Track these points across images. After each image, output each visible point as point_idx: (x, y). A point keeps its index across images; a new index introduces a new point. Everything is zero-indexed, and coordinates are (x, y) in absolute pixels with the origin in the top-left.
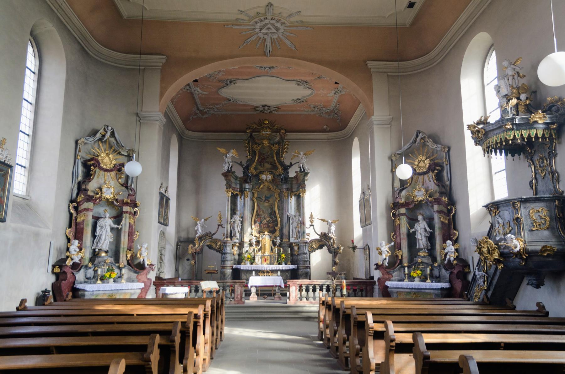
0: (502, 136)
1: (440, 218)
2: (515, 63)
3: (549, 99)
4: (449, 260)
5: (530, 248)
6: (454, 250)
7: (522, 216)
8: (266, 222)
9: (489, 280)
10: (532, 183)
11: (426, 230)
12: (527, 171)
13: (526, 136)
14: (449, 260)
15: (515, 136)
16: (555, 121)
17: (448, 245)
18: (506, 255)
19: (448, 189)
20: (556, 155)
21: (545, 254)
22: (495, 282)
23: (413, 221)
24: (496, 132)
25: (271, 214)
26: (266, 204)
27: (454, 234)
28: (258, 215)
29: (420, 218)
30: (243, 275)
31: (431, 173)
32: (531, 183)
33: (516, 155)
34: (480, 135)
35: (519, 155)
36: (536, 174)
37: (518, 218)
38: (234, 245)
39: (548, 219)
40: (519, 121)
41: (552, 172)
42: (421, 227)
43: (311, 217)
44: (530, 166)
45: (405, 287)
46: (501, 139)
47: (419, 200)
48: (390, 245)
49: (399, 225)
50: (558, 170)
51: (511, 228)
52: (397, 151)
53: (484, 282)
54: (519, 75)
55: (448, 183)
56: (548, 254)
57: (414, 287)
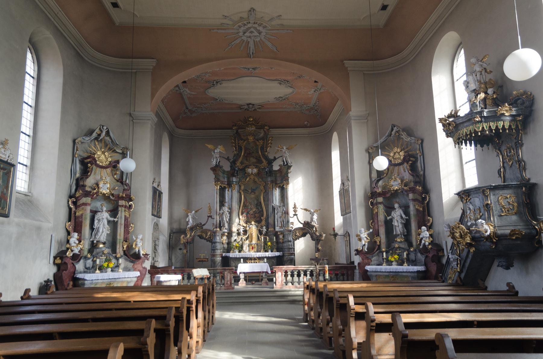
0: (471, 128)
2: (483, 59)
3: (515, 93)
4: (424, 244)
5: (499, 232)
6: (428, 235)
7: (491, 203)
8: (252, 213)
9: (462, 262)
10: (501, 172)
11: (402, 217)
12: (497, 161)
13: (493, 128)
14: (424, 244)
15: (483, 128)
16: (520, 113)
17: (423, 230)
18: (477, 239)
19: (422, 179)
20: (522, 145)
21: (514, 238)
22: (467, 265)
23: (389, 209)
24: (465, 124)
25: (257, 205)
26: (253, 196)
27: (429, 220)
28: (245, 206)
29: (396, 206)
30: (232, 262)
31: (405, 164)
32: (499, 171)
33: (485, 146)
34: (450, 127)
35: (488, 145)
36: (503, 163)
37: (488, 204)
38: (223, 235)
39: (516, 204)
40: (487, 114)
41: (519, 161)
43: (295, 207)
44: (498, 156)
46: (470, 131)
48: (369, 232)
49: (377, 213)
50: (525, 159)
51: (481, 214)
53: (457, 265)
54: (486, 71)
55: (422, 173)
56: (516, 238)
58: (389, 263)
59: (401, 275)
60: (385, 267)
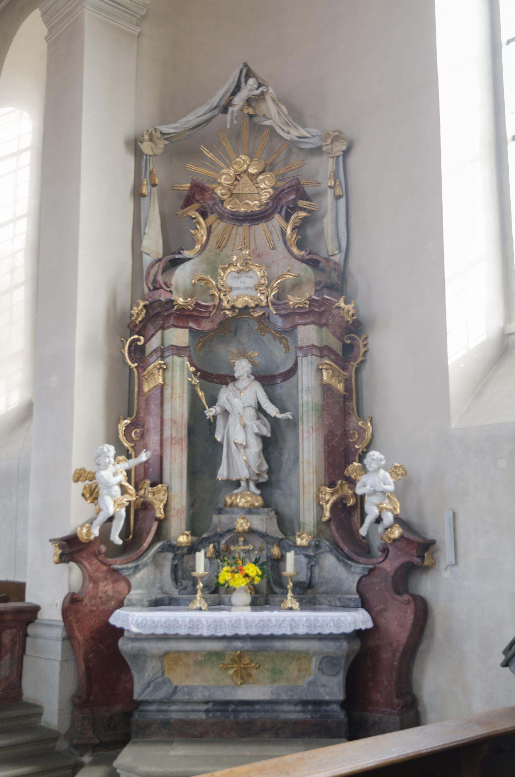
1: (320, 371)
11: (260, 410)
23: (213, 377)
29: (242, 368)
31: (277, 220)
42: (241, 407)
45: (205, 633)
47: (240, 304)
48: (133, 462)
49: (162, 388)
52: (164, 122)
57: (242, 632)
58: (218, 594)
59: (278, 651)
60: (196, 618)
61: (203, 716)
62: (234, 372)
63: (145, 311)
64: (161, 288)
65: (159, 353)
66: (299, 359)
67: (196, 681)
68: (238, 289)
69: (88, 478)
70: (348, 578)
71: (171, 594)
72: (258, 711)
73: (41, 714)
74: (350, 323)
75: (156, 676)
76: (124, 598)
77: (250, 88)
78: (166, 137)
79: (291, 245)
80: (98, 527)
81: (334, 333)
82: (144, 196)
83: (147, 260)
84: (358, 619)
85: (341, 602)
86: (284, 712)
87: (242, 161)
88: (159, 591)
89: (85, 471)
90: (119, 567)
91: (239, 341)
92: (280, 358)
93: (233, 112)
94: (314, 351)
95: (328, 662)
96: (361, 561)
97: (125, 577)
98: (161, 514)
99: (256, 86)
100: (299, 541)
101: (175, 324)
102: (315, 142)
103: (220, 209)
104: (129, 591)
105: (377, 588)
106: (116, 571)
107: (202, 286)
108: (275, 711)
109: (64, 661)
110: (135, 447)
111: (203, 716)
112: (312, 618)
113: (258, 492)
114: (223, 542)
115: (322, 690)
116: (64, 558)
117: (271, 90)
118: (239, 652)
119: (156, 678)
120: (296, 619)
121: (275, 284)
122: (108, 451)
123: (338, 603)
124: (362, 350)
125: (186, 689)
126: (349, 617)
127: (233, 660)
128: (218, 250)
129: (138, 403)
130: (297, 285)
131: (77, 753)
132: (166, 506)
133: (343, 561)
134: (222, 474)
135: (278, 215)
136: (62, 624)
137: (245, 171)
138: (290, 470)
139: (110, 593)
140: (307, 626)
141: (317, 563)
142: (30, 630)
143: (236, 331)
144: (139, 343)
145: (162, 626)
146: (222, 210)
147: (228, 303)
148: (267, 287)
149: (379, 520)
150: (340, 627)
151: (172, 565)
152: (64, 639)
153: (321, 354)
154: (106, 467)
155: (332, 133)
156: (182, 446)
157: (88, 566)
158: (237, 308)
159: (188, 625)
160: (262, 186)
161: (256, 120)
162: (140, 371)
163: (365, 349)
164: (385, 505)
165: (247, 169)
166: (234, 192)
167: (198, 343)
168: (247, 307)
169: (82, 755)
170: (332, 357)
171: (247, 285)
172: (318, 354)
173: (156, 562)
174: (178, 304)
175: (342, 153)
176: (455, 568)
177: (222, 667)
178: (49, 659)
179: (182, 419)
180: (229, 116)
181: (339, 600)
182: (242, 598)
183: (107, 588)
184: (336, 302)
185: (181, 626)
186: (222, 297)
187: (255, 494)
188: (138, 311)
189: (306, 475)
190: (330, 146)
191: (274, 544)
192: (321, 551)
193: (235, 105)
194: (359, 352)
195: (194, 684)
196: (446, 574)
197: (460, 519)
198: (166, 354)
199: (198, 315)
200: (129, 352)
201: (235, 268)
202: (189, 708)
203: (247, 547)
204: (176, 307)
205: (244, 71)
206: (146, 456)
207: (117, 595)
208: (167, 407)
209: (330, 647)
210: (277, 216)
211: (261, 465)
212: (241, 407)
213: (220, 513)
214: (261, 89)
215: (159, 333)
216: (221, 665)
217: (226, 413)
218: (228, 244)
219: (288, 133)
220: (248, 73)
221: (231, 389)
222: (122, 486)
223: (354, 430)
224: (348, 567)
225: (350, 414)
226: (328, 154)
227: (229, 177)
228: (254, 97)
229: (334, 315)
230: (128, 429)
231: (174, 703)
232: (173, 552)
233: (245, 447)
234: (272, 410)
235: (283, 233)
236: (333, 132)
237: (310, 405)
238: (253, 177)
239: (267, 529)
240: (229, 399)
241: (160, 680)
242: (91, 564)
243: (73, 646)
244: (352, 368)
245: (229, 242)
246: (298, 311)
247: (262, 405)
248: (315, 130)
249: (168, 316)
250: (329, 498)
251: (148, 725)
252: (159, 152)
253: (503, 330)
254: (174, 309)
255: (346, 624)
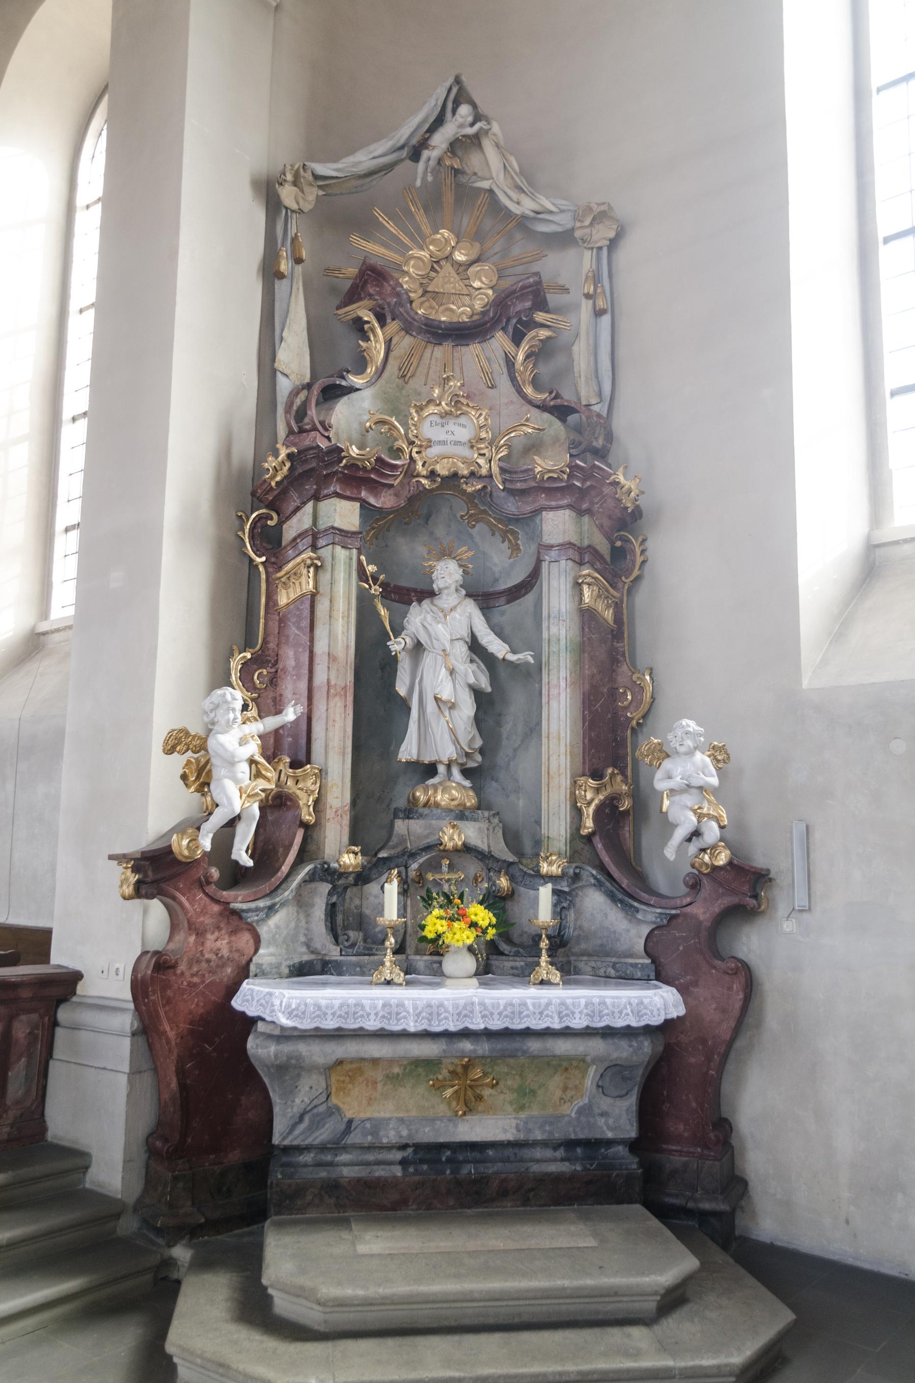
11: (475, 647)
29: (447, 574)
31: (500, 341)
47: (443, 470)
48: (272, 723)
57: (477, 1024)
58: (421, 956)
61: (398, 1171)
62: (432, 582)
63: (288, 465)
64: (315, 429)
65: (309, 540)
66: (545, 565)
67: (385, 1110)
68: (443, 443)
69: (191, 747)
70: (628, 931)
71: (325, 955)
72: (493, 1161)
73: (87, 1168)
74: (630, 510)
75: (315, 1102)
76: (251, 960)
77: (460, 120)
78: (321, 183)
79: (524, 382)
80: (211, 835)
81: (601, 527)
82: (281, 276)
83: (284, 386)
84: (660, 1002)
85: (617, 971)
86: (538, 1161)
87: (443, 240)
88: (304, 949)
89: (187, 734)
90: (244, 906)
91: (432, 533)
92: (504, 565)
93: (429, 159)
94: (571, 552)
95: (615, 1072)
96: (652, 902)
97: (250, 924)
98: (310, 815)
99: (470, 119)
100: (545, 868)
101: (338, 491)
102: (564, 221)
103: (408, 313)
104: (256, 950)
105: (681, 948)
106: (237, 914)
107: (381, 433)
108: (522, 1160)
109: (135, 1072)
110: (259, 700)
111: (398, 1171)
112: (596, 1001)
113: (467, 783)
114: (414, 866)
115: (601, 1121)
116: (141, 891)
117: (496, 128)
118: (466, 1060)
119: (315, 1107)
120: (569, 1001)
121: (502, 442)
122: (234, 699)
123: (612, 972)
124: (639, 559)
125: (368, 1125)
126: (657, 999)
127: (453, 1073)
128: (401, 381)
129: (266, 625)
130: (533, 447)
131: (160, 1241)
132: (317, 802)
133: (621, 901)
134: (408, 751)
135: (501, 333)
136: (131, 1006)
137: (447, 258)
138: (515, 750)
139: (225, 952)
140: (587, 1015)
141: (572, 904)
142: (64, 1014)
143: (428, 518)
144: (269, 522)
145: (334, 1014)
146: (409, 316)
147: (423, 465)
148: (491, 444)
149: (697, 833)
150: (642, 1016)
151: (327, 904)
152: (134, 1034)
153: (581, 559)
154: (229, 725)
155: (596, 206)
156: (345, 701)
157: (186, 904)
158: (439, 475)
159: (381, 1014)
160: (477, 284)
161: (463, 179)
162: (270, 570)
163: (642, 559)
164: (705, 811)
165: (451, 254)
166: (429, 289)
167: (370, 531)
168: (455, 476)
169: (170, 1246)
170: (598, 565)
171: (456, 438)
172: (577, 559)
173: (301, 902)
174: (350, 455)
175: (608, 243)
176: (805, 916)
177: (433, 1085)
178: (104, 1069)
179: (347, 654)
180: (421, 165)
181: (614, 967)
182: (461, 964)
183: (218, 943)
184: (611, 475)
185: (368, 1015)
186: (414, 455)
187: (464, 787)
188: (276, 466)
189: (553, 759)
190: (588, 231)
191: (500, 872)
192: (581, 884)
193: (434, 147)
194: (634, 562)
195: (382, 1115)
196: (788, 926)
197: (817, 836)
198: (321, 542)
199: (378, 479)
200: (252, 537)
201: (438, 408)
202: (370, 1157)
203: (454, 876)
204: (344, 461)
205: (455, 90)
206: (295, 712)
207: (236, 956)
208: (321, 632)
209: (622, 1051)
210: (499, 335)
211: (472, 740)
212: (443, 638)
213: (409, 818)
214: (478, 125)
215: (309, 506)
216: (431, 1082)
217: (418, 648)
218: (418, 373)
219: (518, 203)
220: (459, 95)
221: (428, 609)
222: (252, 762)
223: (626, 687)
224: (630, 911)
225: (618, 661)
226: (584, 241)
227: (421, 263)
228: (464, 139)
229: (604, 497)
230: (247, 668)
231: (345, 1149)
232: (331, 882)
233: (453, 706)
234: (497, 647)
235: (510, 363)
236: (598, 204)
237: (563, 642)
238: (462, 269)
239: (489, 847)
240: (426, 624)
241: (322, 1109)
242: (192, 901)
243: (150, 1047)
244: (624, 587)
245: (419, 369)
246: (547, 485)
247: (480, 639)
248: (564, 202)
249: (326, 476)
250: (591, 797)
251: (299, 1191)
252: (307, 207)
253: (869, 538)
254: (342, 465)
255: (652, 1012)
